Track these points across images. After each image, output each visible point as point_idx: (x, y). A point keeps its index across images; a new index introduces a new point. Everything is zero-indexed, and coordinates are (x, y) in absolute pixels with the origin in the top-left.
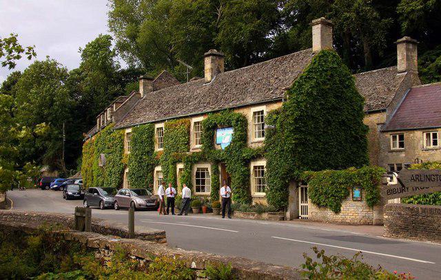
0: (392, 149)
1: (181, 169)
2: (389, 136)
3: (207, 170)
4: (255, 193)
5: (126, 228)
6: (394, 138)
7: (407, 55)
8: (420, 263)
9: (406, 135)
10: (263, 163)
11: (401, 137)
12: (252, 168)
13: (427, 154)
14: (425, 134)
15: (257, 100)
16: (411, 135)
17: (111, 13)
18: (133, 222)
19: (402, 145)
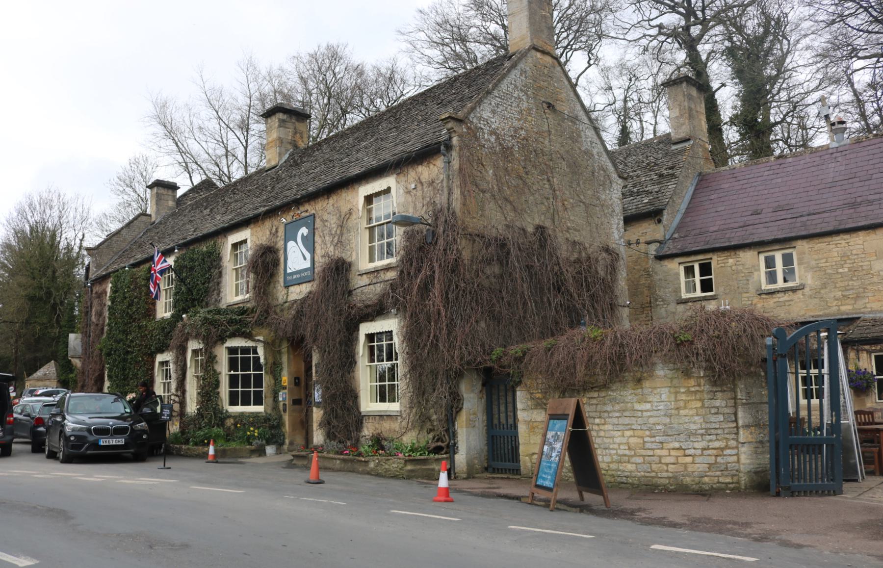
0: (684, 295)
1: (195, 352)
2: (676, 267)
3: (255, 352)
4: (368, 404)
5: (604, 507)
6: (689, 271)
7: (690, 109)
8: (666, 544)
9: (716, 261)
10: (391, 324)
11: (706, 269)
12: (362, 338)
13: (771, 302)
14: (762, 257)
15: (371, 162)
16: (731, 261)
17: (163, 187)
18: (650, 524)
19: (707, 286)
